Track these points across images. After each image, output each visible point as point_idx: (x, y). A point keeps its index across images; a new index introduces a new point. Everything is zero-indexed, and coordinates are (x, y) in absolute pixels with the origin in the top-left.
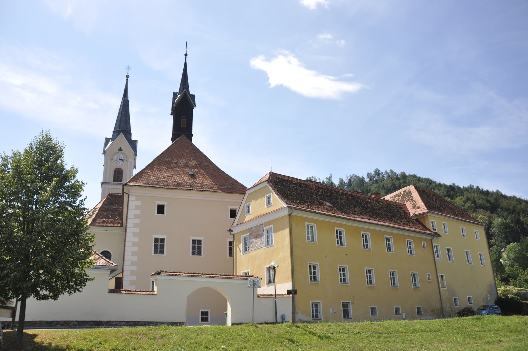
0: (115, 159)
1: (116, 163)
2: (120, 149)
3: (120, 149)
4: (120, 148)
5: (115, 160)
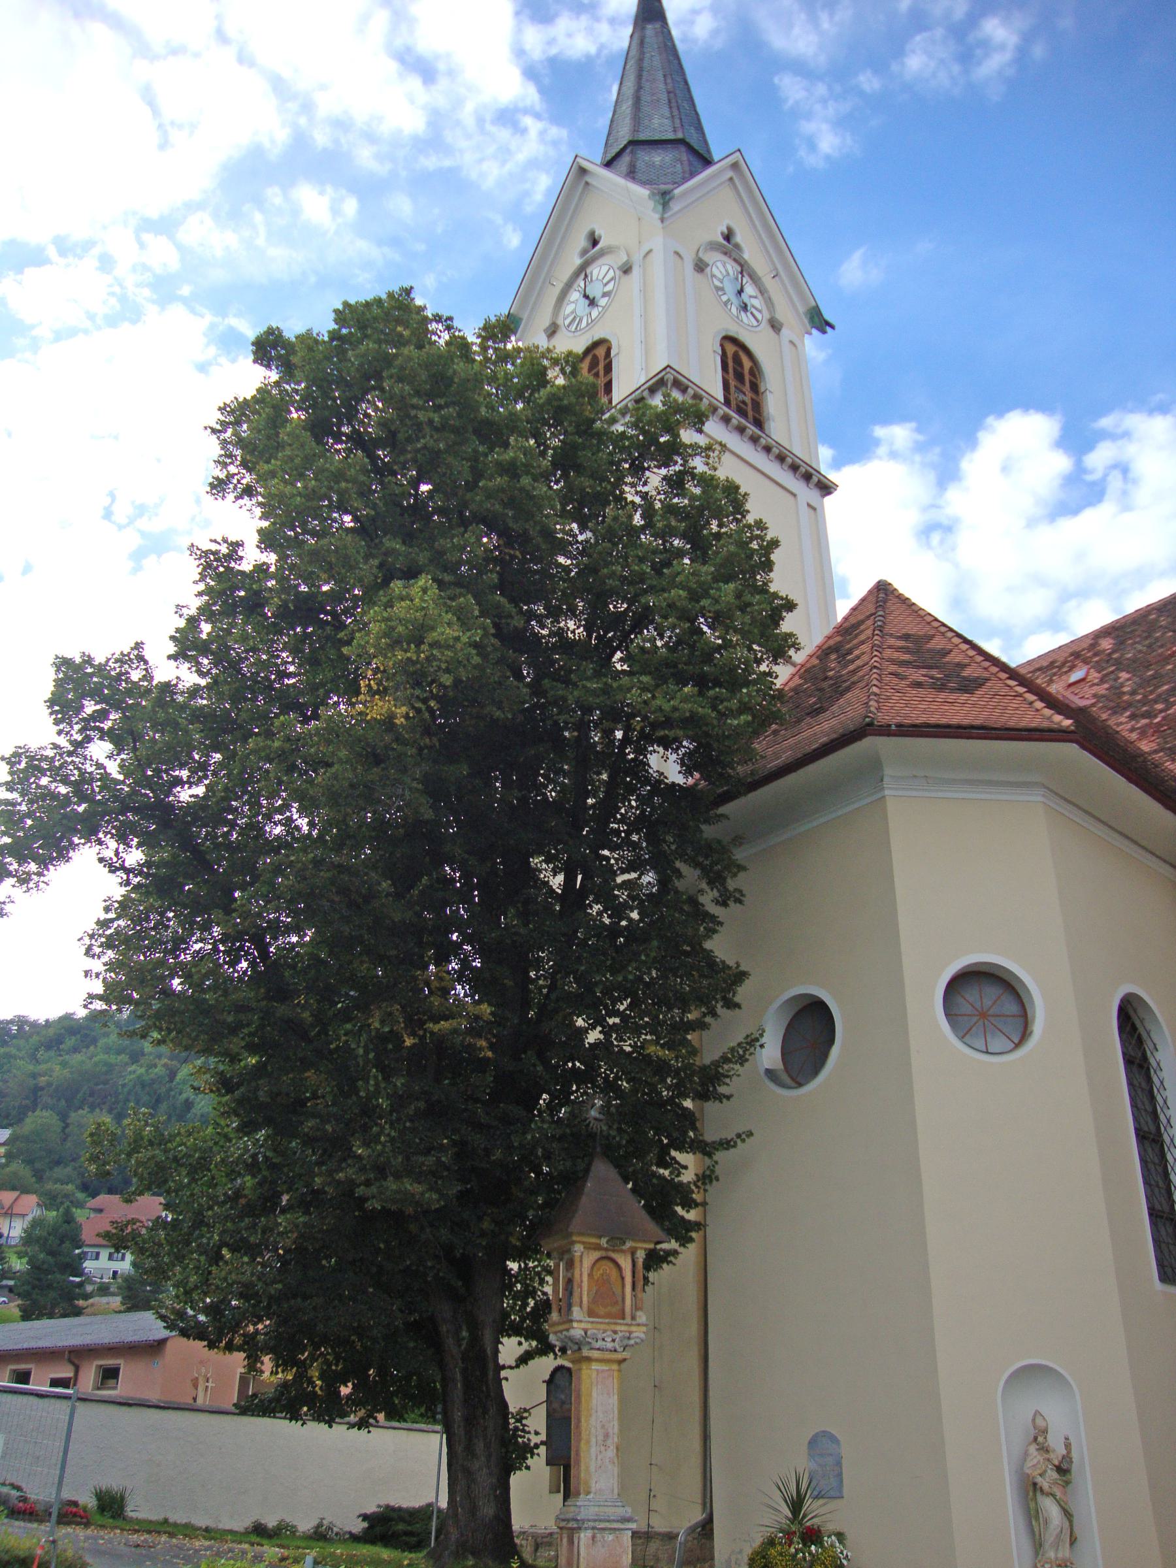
0: (713, 276)
1: (726, 304)
2: (728, 237)
3: (728, 237)
4: (730, 229)
5: (717, 283)
